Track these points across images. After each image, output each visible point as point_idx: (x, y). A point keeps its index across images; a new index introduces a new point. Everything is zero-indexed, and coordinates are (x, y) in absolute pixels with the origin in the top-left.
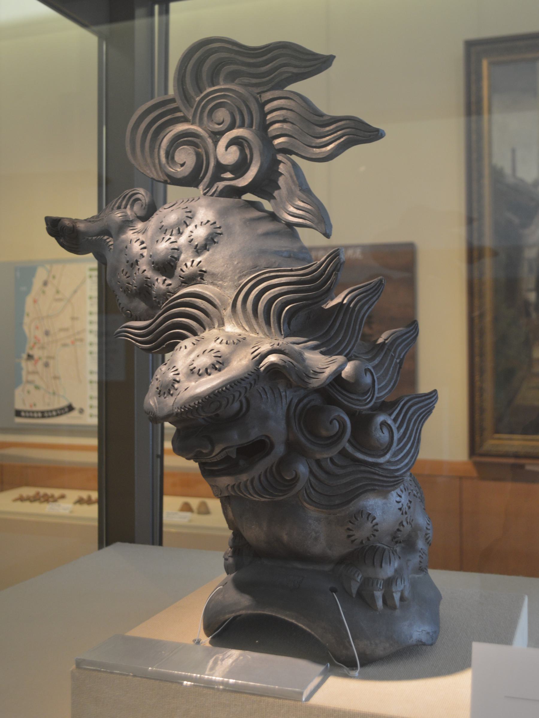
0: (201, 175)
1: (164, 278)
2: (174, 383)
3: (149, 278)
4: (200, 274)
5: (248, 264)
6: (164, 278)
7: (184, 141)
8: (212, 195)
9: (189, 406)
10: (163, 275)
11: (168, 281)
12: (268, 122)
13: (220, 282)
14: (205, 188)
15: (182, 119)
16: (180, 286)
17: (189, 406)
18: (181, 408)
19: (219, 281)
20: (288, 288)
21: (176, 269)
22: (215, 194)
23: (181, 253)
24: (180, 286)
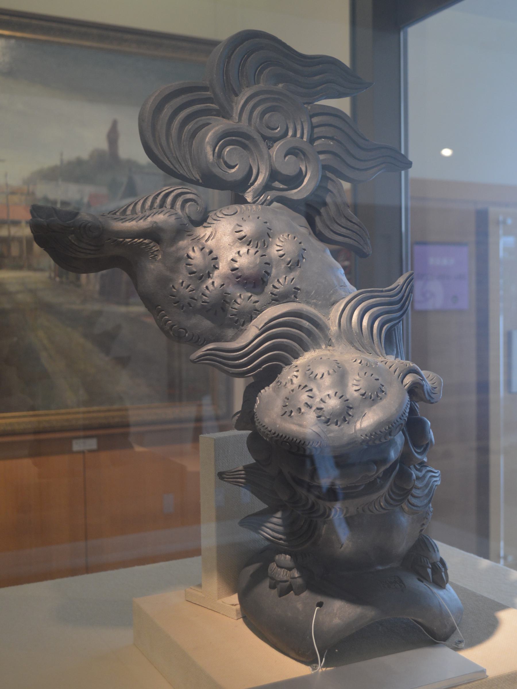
0: (251, 181)
1: (250, 294)
2: (348, 410)
3: (229, 294)
4: (295, 291)
5: (435, 287)
6: (250, 294)
7: (233, 140)
8: (262, 204)
9: (380, 431)
10: (248, 291)
11: (254, 298)
12: (315, 136)
13: (315, 301)
14: (256, 195)
15: (215, 113)
16: (269, 304)
17: (380, 431)
18: (371, 435)
19: (313, 299)
20: (378, 310)
21: (266, 285)
22: (265, 204)
23: (272, 267)
24: (269, 304)
